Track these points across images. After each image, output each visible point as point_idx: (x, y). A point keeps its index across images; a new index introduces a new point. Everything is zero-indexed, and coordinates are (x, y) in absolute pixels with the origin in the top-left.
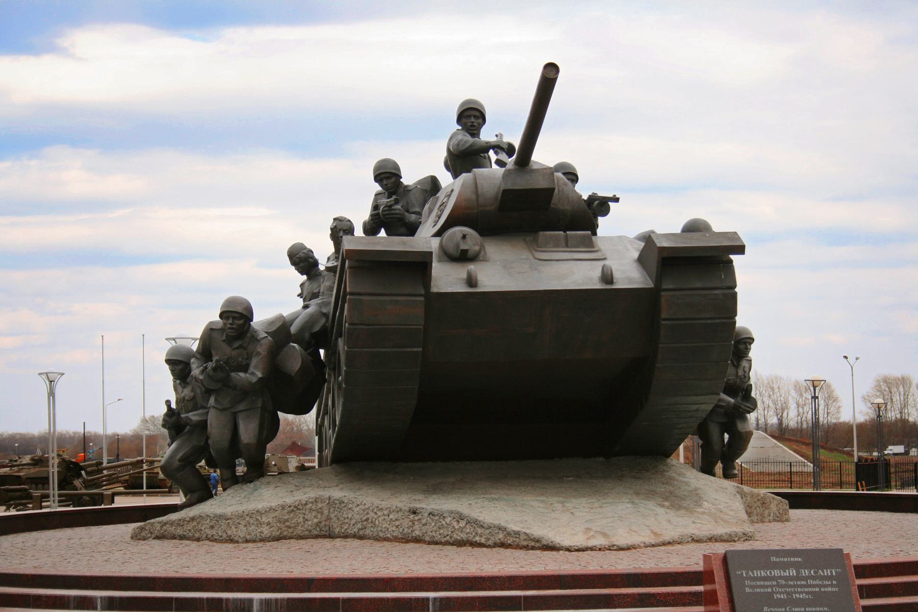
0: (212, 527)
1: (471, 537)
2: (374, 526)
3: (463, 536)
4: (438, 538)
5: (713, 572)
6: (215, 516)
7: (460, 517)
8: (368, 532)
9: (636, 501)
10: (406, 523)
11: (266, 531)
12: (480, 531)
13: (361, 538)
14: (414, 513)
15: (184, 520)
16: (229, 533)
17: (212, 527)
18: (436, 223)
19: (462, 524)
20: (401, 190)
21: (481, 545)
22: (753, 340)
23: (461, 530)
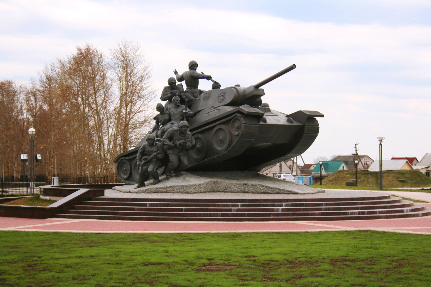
0: (179, 189)
1: (267, 191)
2: (230, 188)
3: (264, 191)
4: (254, 191)
5: (59, 182)
6: (181, 186)
7: (263, 186)
8: (228, 190)
9: (131, 64)
10: (242, 188)
11: (202, 190)
12: (270, 189)
13: (225, 192)
14: (245, 185)
15: (167, 187)
16: (187, 190)
17: (179, 189)
18: (323, 192)
19: (263, 188)
20: (74, 83)
21: (270, 193)
22: (197, 64)
23: (263, 189)
